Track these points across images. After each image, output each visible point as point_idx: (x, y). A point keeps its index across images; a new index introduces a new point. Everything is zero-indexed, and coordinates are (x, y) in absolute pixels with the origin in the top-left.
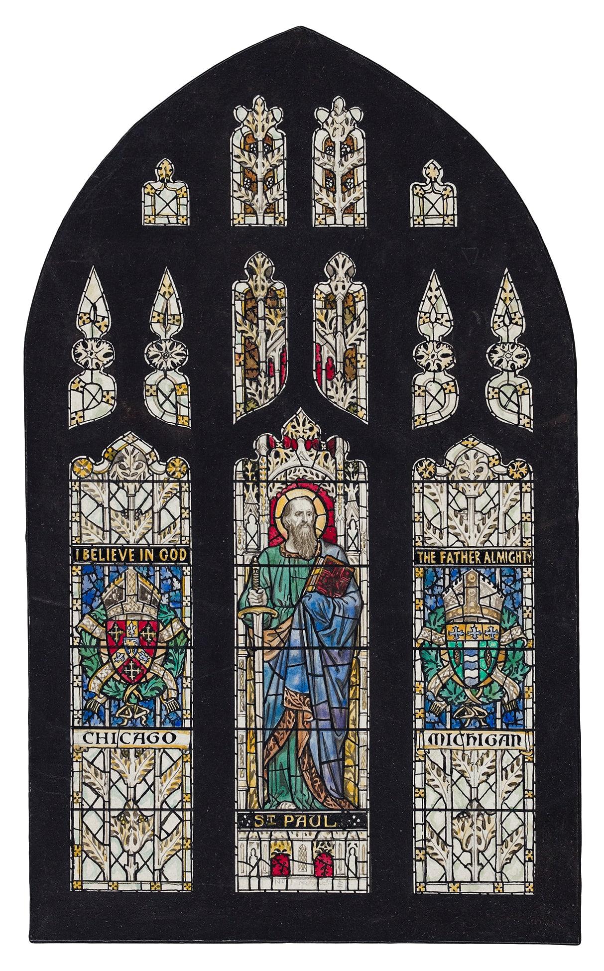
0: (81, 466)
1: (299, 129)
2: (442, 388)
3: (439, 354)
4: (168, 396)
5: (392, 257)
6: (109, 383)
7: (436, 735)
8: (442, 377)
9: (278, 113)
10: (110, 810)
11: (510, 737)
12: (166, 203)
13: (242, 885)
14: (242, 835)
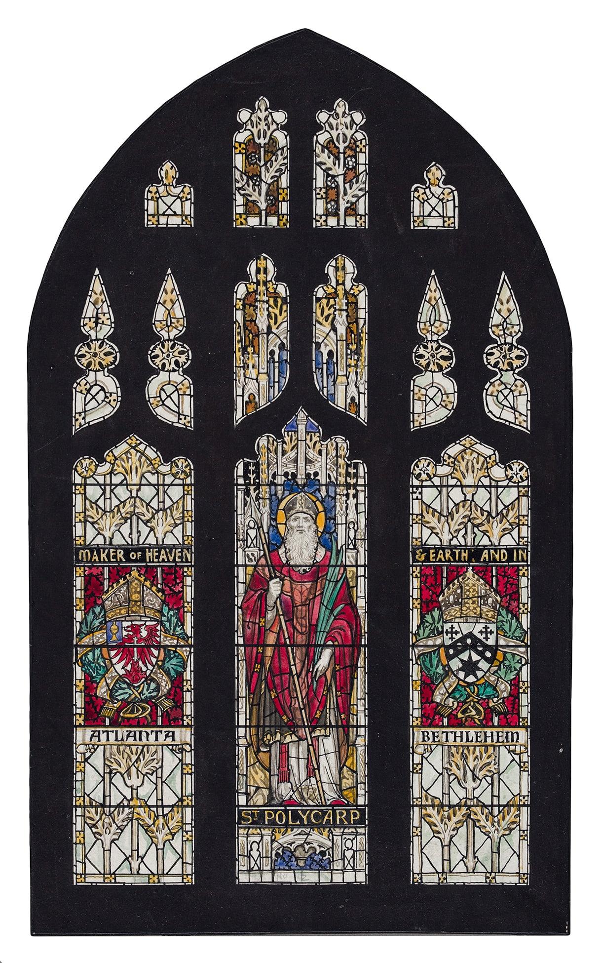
0: (423, 464)
1: (302, 131)
2: (177, 390)
3: (438, 356)
4: (172, 397)
5: (393, 258)
6: (111, 384)
7: (140, 732)
8: (176, 377)
9: (244, 115)
10: (163, 806)
11: (138, 733)
12: (170, 204)
13: (361, 878)
14: (241, 831)
